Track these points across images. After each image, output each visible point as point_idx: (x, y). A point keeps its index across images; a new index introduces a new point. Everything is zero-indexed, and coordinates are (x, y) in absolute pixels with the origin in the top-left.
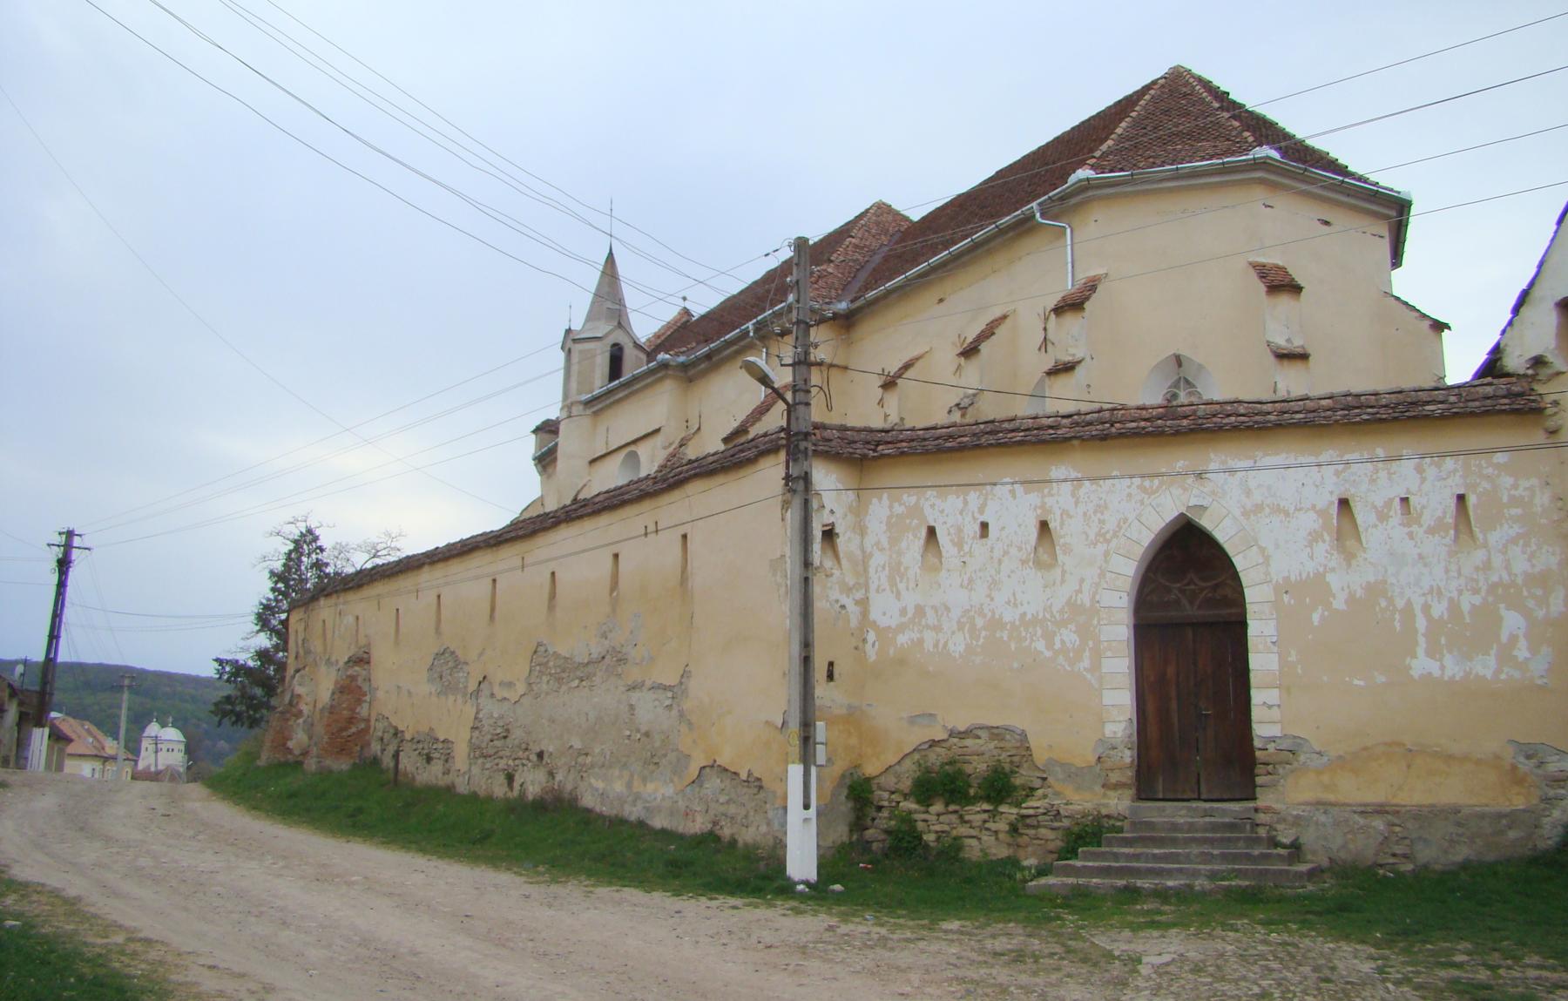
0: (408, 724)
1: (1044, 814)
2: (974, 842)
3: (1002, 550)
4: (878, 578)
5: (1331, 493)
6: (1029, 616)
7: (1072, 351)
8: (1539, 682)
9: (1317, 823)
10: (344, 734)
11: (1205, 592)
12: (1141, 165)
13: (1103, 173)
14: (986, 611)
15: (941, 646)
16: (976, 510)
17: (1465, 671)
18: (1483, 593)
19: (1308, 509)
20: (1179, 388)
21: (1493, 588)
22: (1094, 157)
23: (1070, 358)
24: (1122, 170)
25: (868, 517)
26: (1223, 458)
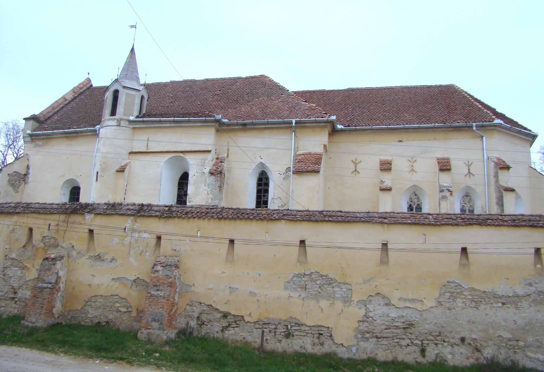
7: (508, 184)
23: (508, 186)
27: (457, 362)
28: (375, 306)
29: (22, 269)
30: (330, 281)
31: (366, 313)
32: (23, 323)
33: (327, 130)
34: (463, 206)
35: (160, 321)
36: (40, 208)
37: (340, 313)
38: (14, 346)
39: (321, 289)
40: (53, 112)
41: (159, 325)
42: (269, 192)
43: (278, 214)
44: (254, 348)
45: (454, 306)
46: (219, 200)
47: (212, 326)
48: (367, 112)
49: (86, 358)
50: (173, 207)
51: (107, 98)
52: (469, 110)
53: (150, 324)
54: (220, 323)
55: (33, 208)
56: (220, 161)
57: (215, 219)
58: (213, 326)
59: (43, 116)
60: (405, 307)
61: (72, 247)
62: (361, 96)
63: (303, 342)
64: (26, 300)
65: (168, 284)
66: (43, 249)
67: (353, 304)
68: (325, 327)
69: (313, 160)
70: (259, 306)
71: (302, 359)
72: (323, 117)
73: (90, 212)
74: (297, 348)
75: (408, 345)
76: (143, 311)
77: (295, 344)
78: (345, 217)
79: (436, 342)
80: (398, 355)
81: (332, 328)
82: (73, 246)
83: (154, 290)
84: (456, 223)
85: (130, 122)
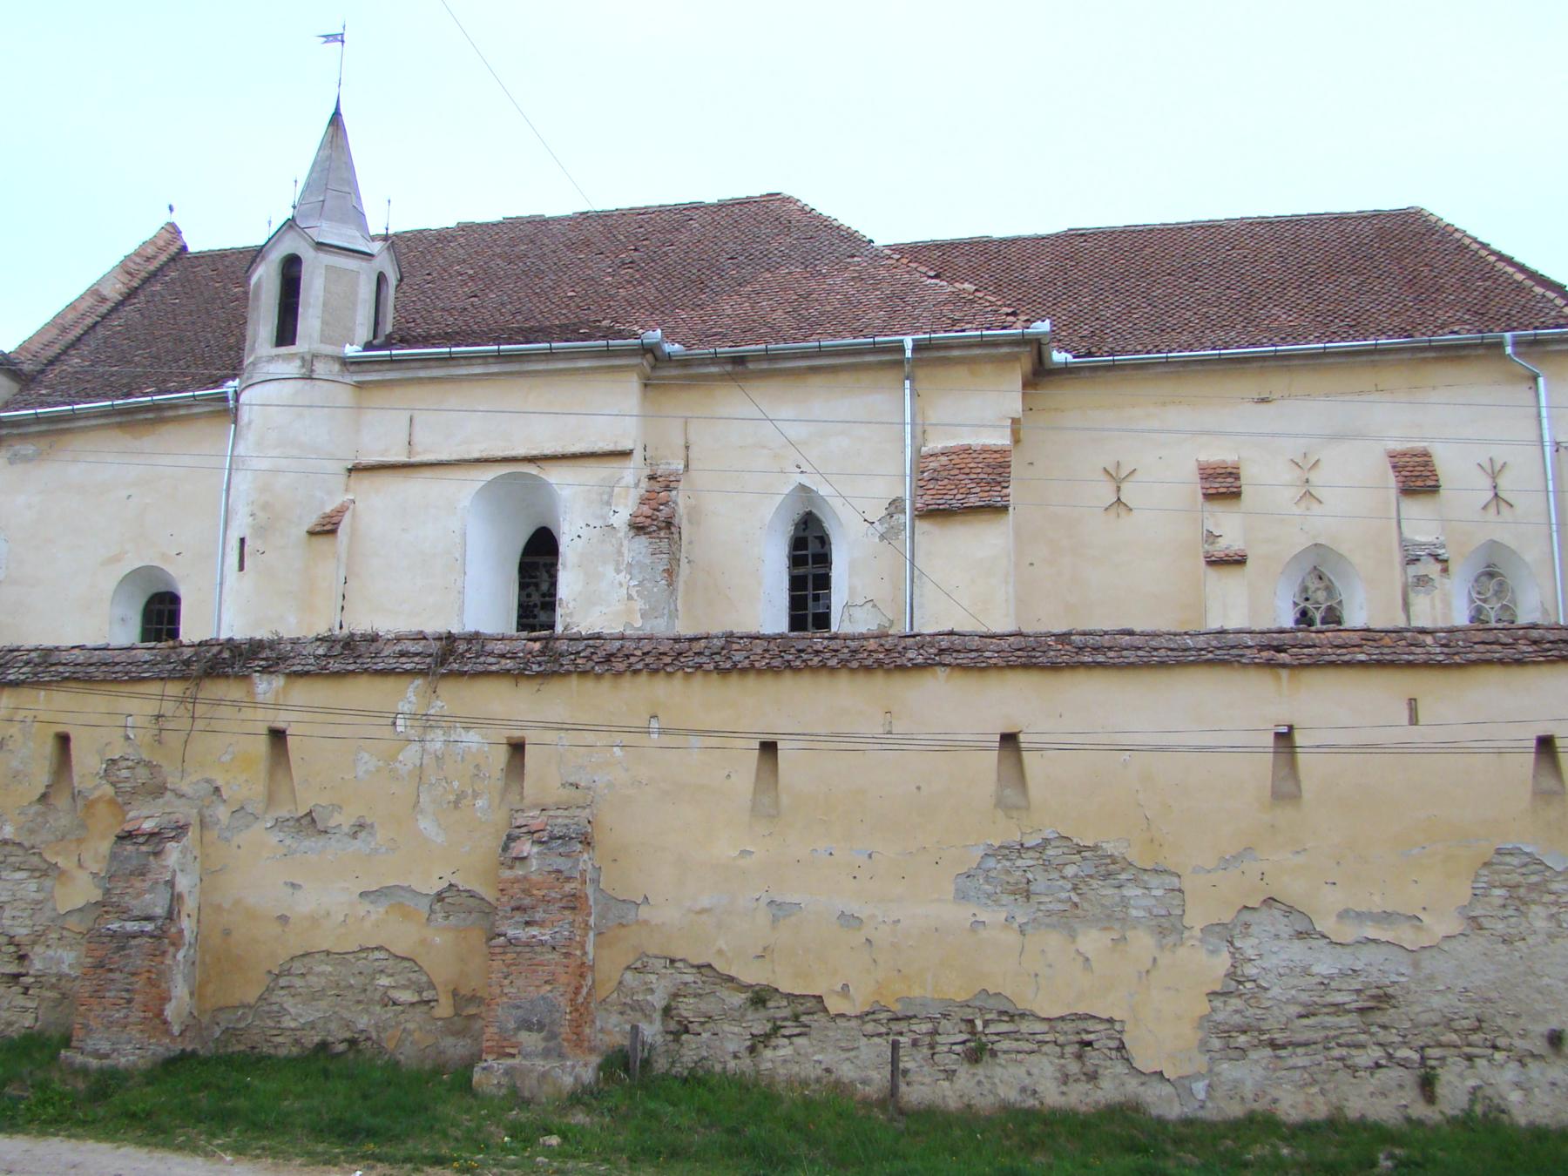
27: (1540, 1113)
28: (1261, 943)
29: (41, 876)
30: (1107, 864)
31: (1232, 966)
32: (67, 1057)
33: (1020, 372)
34: (1479, 610)
35: (547, 1028)
36: (91, 665)
37: (1148, 972)
38: (56, 1135)
39: (1078, 894)
40: (62, 342)
41: (545, 1039)
42: (833, 586)
43: (922, 647)
44: (866, 1103)
45: (1521, 929)
46: (670, 617)
47: (715, 1037)
48: (1144, 305)
49: (313, 1165)
50: (557, 639)
51: (258, 285)
52: (1485, 289)
53: (513, 1040)
54: (744, 1025)
55: (65, 664)
56: (663, 484)
57: (708, 672)
58: (721, 1035)
59: (30, 357)
60: (1359, 939)
61: (214, 792)
62: (1117, 254)
63: (1029, 1074)
64: (63, 982)
65: (564, 901)
66: (112, 802)
67: (1192, 937)
68: (1101, 1020)
69: (979, 470)
70: (875, 961)
71: (1035, 1128)
72: (1005, 324)
73: (272, 670)
74: (1013, 1096)
75: (1378, 1066)
76: (473, 999)
77: (1001, 1082)
78: (1147, 649)
79: (1467, 1050)
80: (1347, 1100)
81: (1122, 1021)
82: (217, 789)
83: (516, 925)
84: (1516, 656)
85: (347, 363)
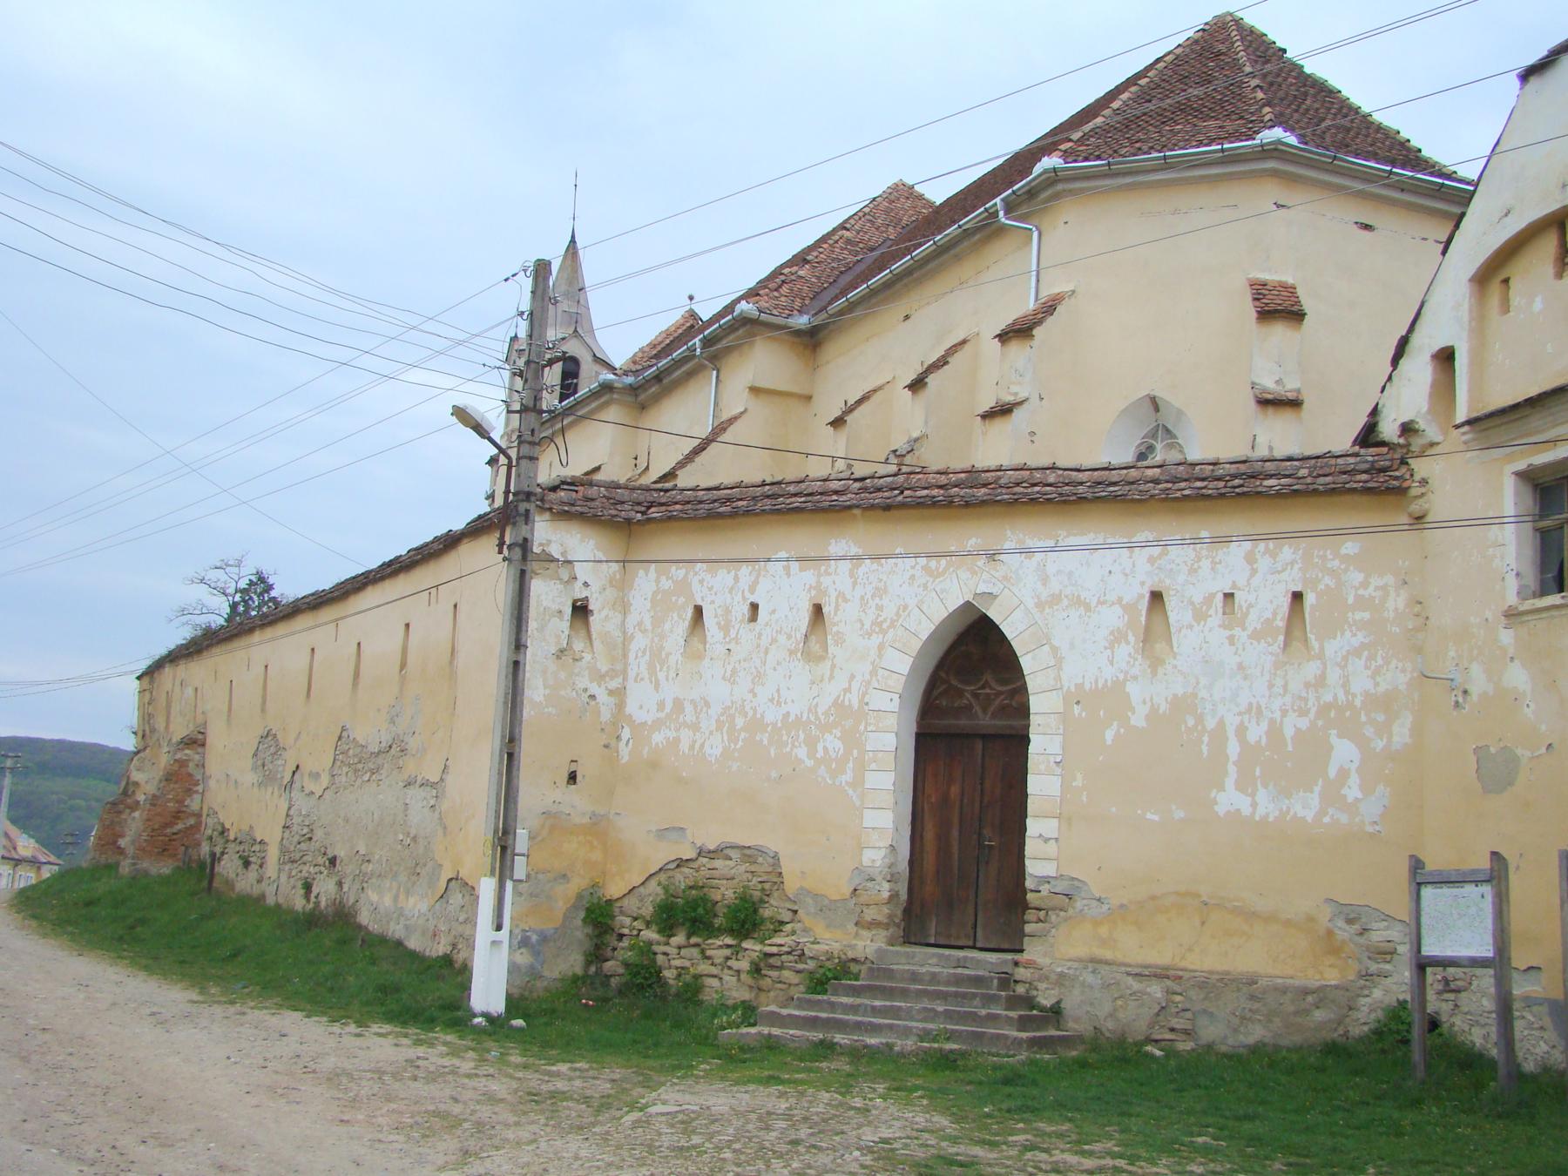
0: (234, 821)
1: (789, 953)
2: (714, 982)
3: (770, 637)
4: (638, 664)
5: (1143, 583)
6: (792, 717)
7: (1014, 389)
8: (1370, 829)
9: (1083, 984)
10: (169, 831)
11: (1002, 697)
12: (1123, 151)
13: (1075, 161)
14: (747, 708)
15: (697, 746)
16: (747, 588)
17: (1281, 810)
18: (1312, 715)
19: (1113, 604)
20: (1156, 440)
21: (1324, 710)
22: (1070, 140)
24: (1098, 158)
25: (633, 592)
26: (1021, 536)
